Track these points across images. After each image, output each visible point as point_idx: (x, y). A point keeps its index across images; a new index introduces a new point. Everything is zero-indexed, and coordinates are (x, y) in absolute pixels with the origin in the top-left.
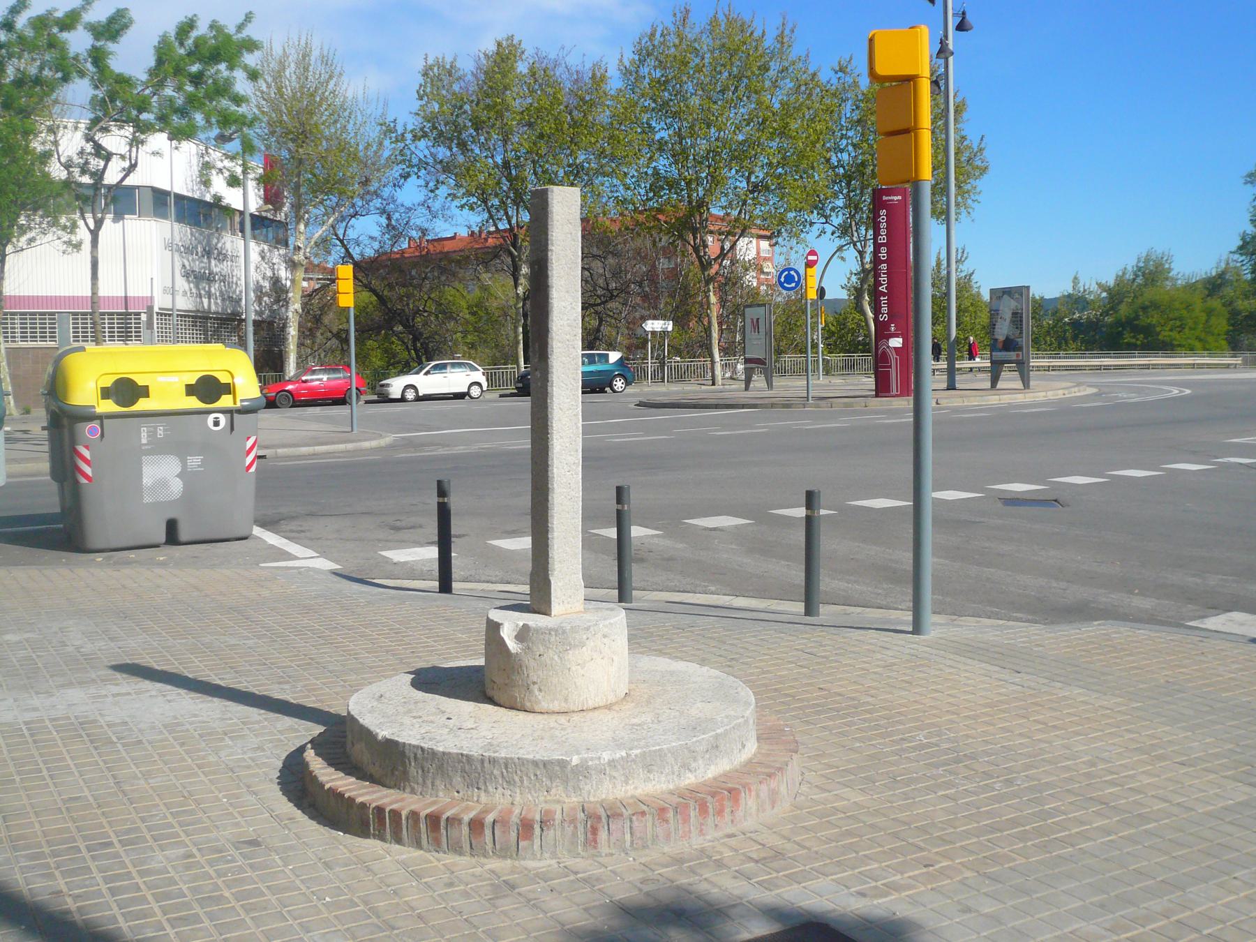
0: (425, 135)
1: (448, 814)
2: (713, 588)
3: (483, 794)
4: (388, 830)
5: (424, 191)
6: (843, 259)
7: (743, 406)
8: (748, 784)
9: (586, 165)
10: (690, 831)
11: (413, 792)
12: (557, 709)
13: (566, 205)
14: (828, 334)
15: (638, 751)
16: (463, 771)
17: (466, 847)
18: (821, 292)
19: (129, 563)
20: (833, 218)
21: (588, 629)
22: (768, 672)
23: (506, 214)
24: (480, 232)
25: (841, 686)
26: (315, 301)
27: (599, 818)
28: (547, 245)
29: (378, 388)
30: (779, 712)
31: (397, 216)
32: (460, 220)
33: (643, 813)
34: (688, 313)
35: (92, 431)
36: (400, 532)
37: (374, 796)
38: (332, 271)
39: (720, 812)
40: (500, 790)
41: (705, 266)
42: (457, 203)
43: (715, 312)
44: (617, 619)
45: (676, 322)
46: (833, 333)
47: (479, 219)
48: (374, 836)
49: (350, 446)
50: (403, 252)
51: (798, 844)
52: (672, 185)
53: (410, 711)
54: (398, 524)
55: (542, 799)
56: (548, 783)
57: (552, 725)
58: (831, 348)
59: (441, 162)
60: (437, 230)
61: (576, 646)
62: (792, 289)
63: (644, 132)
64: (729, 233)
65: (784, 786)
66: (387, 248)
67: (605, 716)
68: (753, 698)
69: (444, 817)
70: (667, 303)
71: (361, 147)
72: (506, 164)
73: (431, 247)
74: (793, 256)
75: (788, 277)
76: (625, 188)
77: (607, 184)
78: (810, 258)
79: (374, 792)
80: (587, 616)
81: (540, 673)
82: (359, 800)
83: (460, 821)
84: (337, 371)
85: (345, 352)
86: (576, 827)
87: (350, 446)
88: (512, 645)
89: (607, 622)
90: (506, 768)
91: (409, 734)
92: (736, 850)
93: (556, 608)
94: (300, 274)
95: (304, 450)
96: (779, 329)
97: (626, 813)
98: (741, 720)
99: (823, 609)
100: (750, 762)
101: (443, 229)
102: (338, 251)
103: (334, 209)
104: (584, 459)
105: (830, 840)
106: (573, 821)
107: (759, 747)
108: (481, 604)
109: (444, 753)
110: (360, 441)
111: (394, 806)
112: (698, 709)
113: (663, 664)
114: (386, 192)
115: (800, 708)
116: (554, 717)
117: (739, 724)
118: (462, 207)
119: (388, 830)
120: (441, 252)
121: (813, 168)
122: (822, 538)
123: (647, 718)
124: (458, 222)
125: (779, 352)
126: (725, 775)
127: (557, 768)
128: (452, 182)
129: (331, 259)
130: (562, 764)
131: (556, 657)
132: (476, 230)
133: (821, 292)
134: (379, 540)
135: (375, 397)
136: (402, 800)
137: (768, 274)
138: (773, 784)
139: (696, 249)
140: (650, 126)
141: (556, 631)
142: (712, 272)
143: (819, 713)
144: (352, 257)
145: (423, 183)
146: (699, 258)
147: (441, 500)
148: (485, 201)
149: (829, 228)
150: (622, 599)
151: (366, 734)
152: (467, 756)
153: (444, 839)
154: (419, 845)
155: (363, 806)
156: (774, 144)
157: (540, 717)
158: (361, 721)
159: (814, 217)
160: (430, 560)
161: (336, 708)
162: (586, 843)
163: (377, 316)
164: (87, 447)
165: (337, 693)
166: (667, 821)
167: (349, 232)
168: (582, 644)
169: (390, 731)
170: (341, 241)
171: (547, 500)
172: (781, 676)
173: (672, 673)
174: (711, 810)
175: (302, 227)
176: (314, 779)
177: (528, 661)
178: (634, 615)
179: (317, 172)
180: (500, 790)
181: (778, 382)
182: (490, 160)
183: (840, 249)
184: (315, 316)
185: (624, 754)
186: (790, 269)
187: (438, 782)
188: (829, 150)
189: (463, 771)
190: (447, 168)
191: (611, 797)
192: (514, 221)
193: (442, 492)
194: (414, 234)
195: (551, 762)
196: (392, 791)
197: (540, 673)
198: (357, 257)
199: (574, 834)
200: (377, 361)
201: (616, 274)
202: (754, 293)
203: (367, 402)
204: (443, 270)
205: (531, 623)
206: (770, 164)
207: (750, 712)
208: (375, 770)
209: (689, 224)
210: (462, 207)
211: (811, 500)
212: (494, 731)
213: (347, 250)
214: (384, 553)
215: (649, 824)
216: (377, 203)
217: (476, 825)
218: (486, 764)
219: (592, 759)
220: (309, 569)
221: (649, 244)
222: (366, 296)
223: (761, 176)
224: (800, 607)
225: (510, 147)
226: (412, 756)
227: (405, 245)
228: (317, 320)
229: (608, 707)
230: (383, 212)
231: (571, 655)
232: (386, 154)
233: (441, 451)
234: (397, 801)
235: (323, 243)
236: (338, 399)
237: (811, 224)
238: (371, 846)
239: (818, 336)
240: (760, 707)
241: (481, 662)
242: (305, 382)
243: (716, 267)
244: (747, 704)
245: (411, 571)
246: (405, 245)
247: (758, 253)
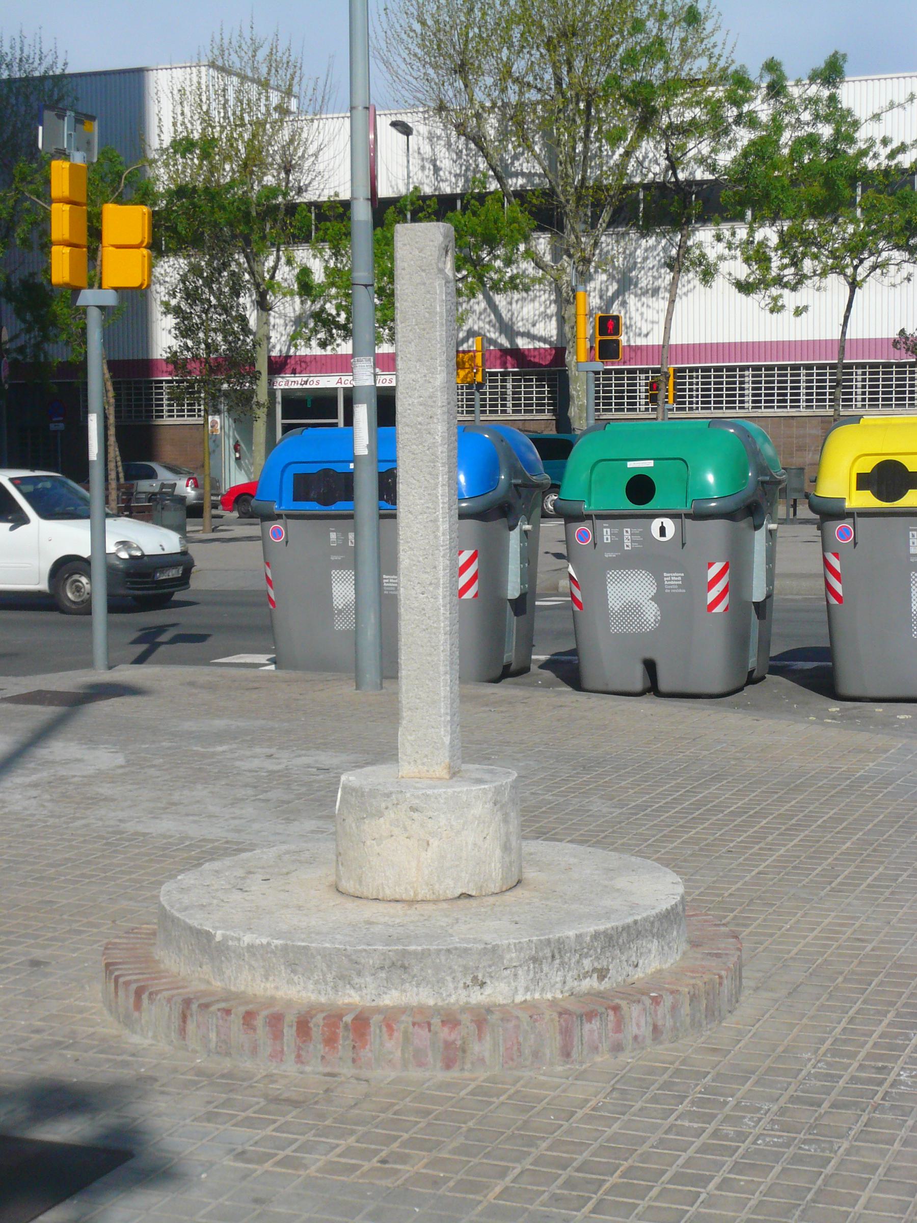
19: (886, 724)
21: (389, 795)
35: (843, 533)
164: (836, 555)
166: (254, 1029)
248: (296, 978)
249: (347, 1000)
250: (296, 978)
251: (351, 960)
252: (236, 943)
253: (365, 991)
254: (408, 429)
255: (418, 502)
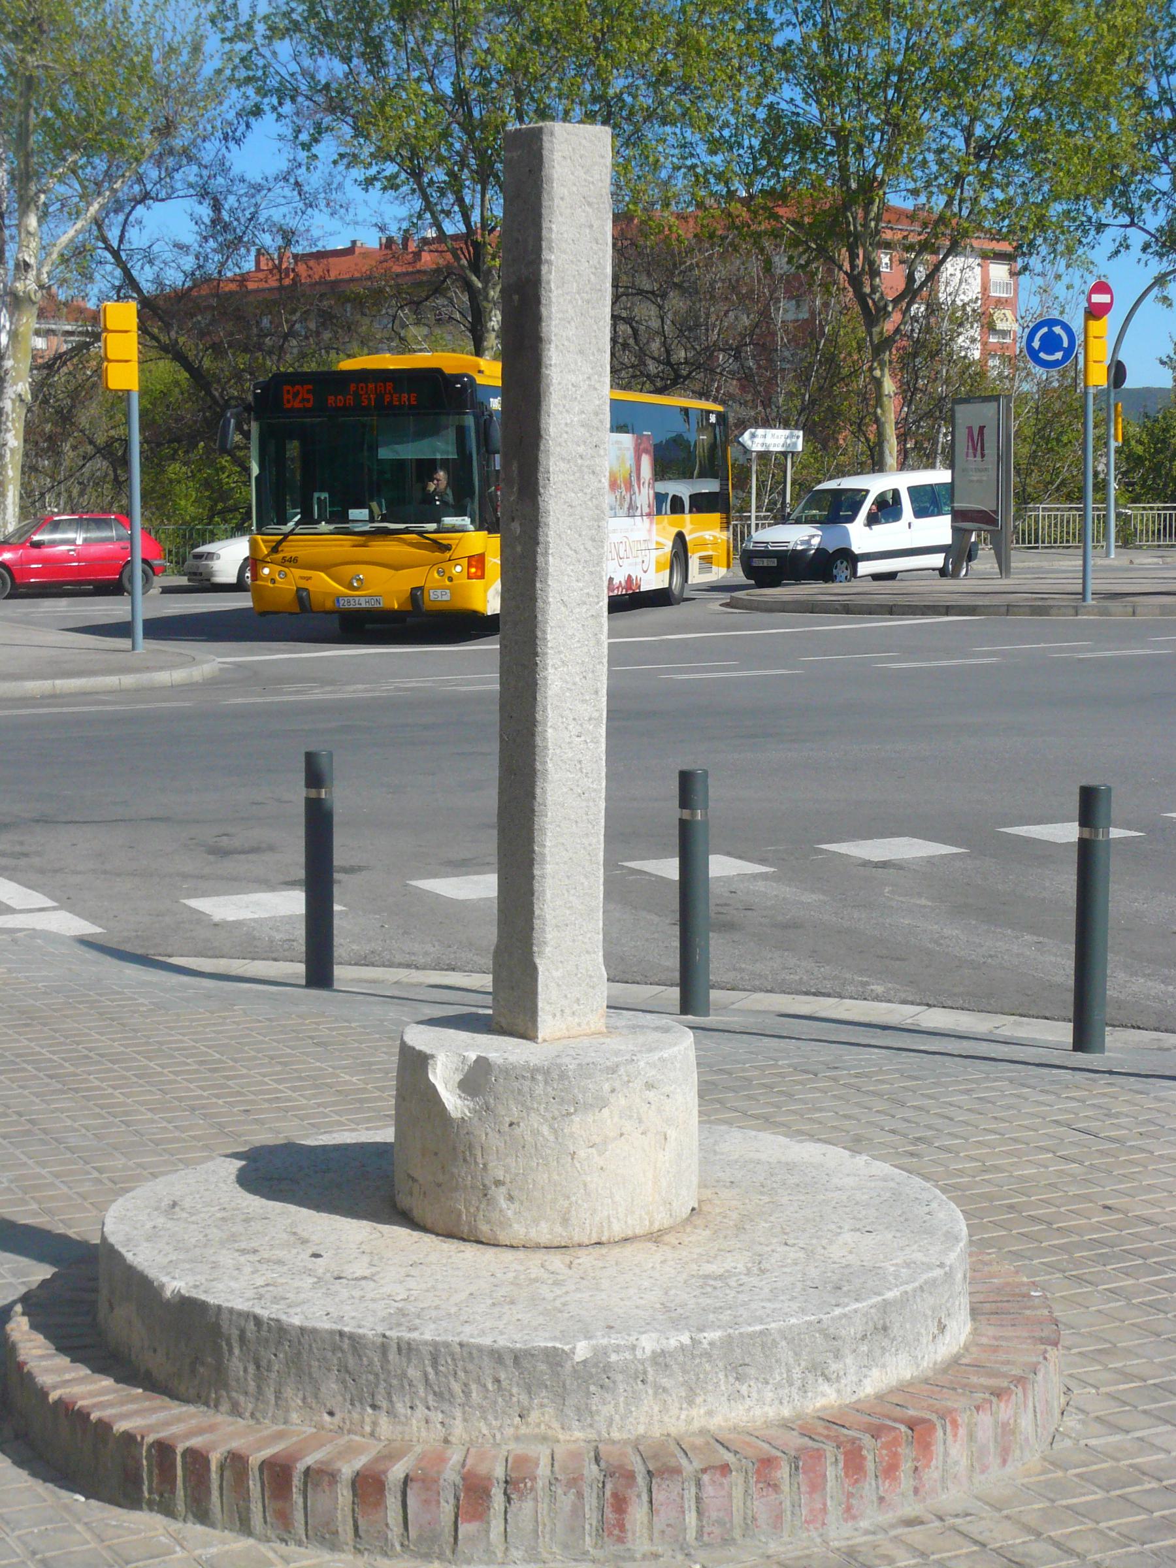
0: (296, 27)
1: (309, 1460)
2: (879, 989)
3: (384, 1420)
4: (180, 1492)
5: (288, 152)
6: (1165, 299)
7: (947, 610)
8: (950, 1411)
9: (628, 99)
10: (824, 1509)
11: (236, 1411)
12: (544, 1239)
13: (580, 165)
14: (1130, 460)
15: (715, 1335)
16: (344, 1368)
17: (346, 1531)
18: (1118, 372)
20: (1148, 215)
21: (613, 1070)
22: (997, 1169)
23: (460, 201)
24: (406, 240)
25: (1153, 1203)
26: (59, 378)
27: (630, 1476)
28: (538, 250)
29: (190, 562)
30: (1017, 1255)
31: (231, 201)
32: (363, 213)
33: (725, 1469)
34: (834, 415)
36: (227, 861)
37: (153, 1419)
38: (96, 317)
39: (890, 1470)
40: (421, 1410)
41: (872, 315)
42: (358, 173)
43: (891, 412)
44: (680, 1047)
45: (810, 433)
46: (1139, 460)
47: (403, 211)
48: (151, 1506)
49: (128, 680)
50: (243, 279)
51: (1057, 1544)
52: (805, 142)
53: (233, 1238)
54: (225, 842)
55: (509, 1432)
56: (524, 1397)
57: (535, 1272)
58: (1134, 493)
59: (327, 86)
60: (316, 233)
61: (587, 1107)
62: (1056, 363)
63: (749, 28)
64: (925, 247)
65: (1031, 1415)
66: (211, 268)
67: (647, 1257)
68: (962, 1228)
69: (300, 1467)
70: (790, 394)
71: (156, 55)
72: (461, 95)
73: (301, 268)
74: (1059, 289)
75: (1050, 341)
76: (698, 159)
77: (671, 140)
78: (1097, 298)
79: (153, 1410)
80: (614, 1043)
81: (511, 1161)
82: (120, 1427)
83: (333, 1477)
84: (106, 524)
85: (121, 485)
86: (580, 1495)
87: (128, 680)
88: (453, 1101)
89: (656, 1056)
90: (435, 1363)
91: (230, 1289)
92: (923, 1554)
93: (548, 1024)
94: (29, 320)
95: (33, 687)
96: (1025, 450)
97: (688, 1468)
98: (938, 1272)
99: (1114, 1038)
100: (955, 1362)
101: (328, 232)
102: (107, 274)
103: (98, 184)
104: (615, 714)
105: (1127, 1539)
106: (574, 1482)
107: (975, 1332)
108: (393, 1012)
109: (302, 1330)
110: (148, 669)
111: (195, 1442)
112: (846, 1247)
113: (771, 1147)
114: (210, 150)
115: (1062, 1248)
116: (538, 1257)
117: (933, 1282)
118: (369, 182)
119: (180, 1492)
120: (322, 282)
121: (1106, 107)
122: (1113, 887)
123: (737, 1262)
124: (359, 216)
125: (1024, 498)
126: (902, 1388)
127: (543, 1367)
128: (347, 130)
129: (94, 290)
130: (554, 1358)
131: (545, 1130)
132: (398, 237)
133: (1118, 372)
134: (185, 876)
135: (183, 581)
136: (211, 1428)
137: (1004, 333)
138: (1004, 1411)
139: (855, 281)
140: (762, 17)
141: (547, 1072)
142: (889, 326)
143: (1104, 1260)
144: (138, 290)
145: (288, 132)
146: (861, 298)
147: (313, 793)
148: (416, 174)
149: (1137, 238)
150: (687, 1005)
151: (140, 1287)
152: (352, 1337)
153: (299, 1516)
154: (245, 1528)
155: (129, 1438)
156: (1025, 57)
157: (508, 1256)
158: (129, 1257)
159: (1106, 212)
160: (289, 919)
161: (80, 1228)
162: (602, 1528)
163: (189, 412)
165: (84, 1197)
166: (776, 1487)
167: (132, 233)
168: (601, 1103)
169: (191, 1280)
170: (116, 254)
171: (532, 796)
172: (1022, 1179)
173: (790, 1167)
174: (870, 1465)
175: (32, 221)
176: (26, 1379)
177: (488, 1137)
178: (711, 1041)
179: (64, 105)
180: (421, 1410)
181: (1021, 560)
182: (427, 87)
183: (1161, 280)
184: (59, 412)
185: (685, 1339)
186: (1051, 323)
187: (288, 1392)
188: (1141, 68)
189: (344, 1368)
190: (335, 101)
191: (656, 1432)
192: (475, 217)
193: (315, 776)
194: (267, 240)
195: (529, 1354)
196: (191, 1409)
197: (511, 1161)
198: (147, 287)
199: (577, 1511)
200: (188, 505)
201: (688, 327)
202: (973, 375)
203: (167, 590)
204: (327, 318)
205: (493, 1056)
206: (1017, 101)
207: (956, 1255)
208: (156, 1363)
209: (839, 227)
210: (369, 182)
211: (1090, 806)
212: (411, 1283)
213: (127, 273)
214: (194, 903)
215: (738, 1493)
216: (191, 172)
217: (368, 1486)
218: (392, 1356)
219: (617, 1349)
220: (34, 933)
221: (755, 267)
222: (166, 368)
223: (997, 123)
224: (1064, 1032)
225: (468, 59)
226: (235, 1333)
227: (249, 265)
228: (65, 418)
229: (655, 1237)
230: (204, 193)
231: (577, 1125)
232: (208, 70)
233: (318, 695)
234: (200, 1431)
235: (77, 255)
236: (107, 581)
237: (1100, 227)
238: (143, 1526)
239: (1107, 465)
240: (978, 1245)
241: (386, 1135)
242: (38, 545)
243: (896, 317)
244: (951, 1237)
245: (249, 941)
246: (249, 265)
247: (985, 288)
248: (744, 1389)
249: (820, 1402)
250: (744, 1389)
251: (826, 1336)
252: (628, 1355)
253: (843, 1381)
254: (563, 466)
255: (575, 585)
